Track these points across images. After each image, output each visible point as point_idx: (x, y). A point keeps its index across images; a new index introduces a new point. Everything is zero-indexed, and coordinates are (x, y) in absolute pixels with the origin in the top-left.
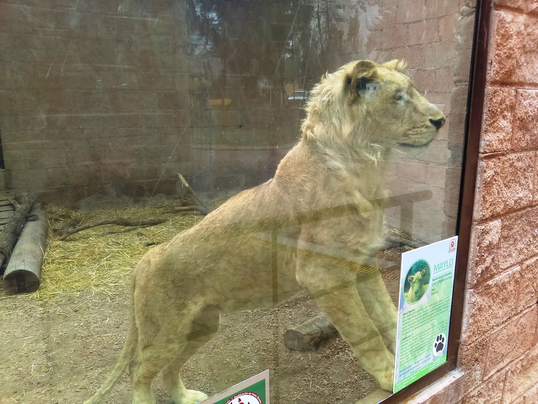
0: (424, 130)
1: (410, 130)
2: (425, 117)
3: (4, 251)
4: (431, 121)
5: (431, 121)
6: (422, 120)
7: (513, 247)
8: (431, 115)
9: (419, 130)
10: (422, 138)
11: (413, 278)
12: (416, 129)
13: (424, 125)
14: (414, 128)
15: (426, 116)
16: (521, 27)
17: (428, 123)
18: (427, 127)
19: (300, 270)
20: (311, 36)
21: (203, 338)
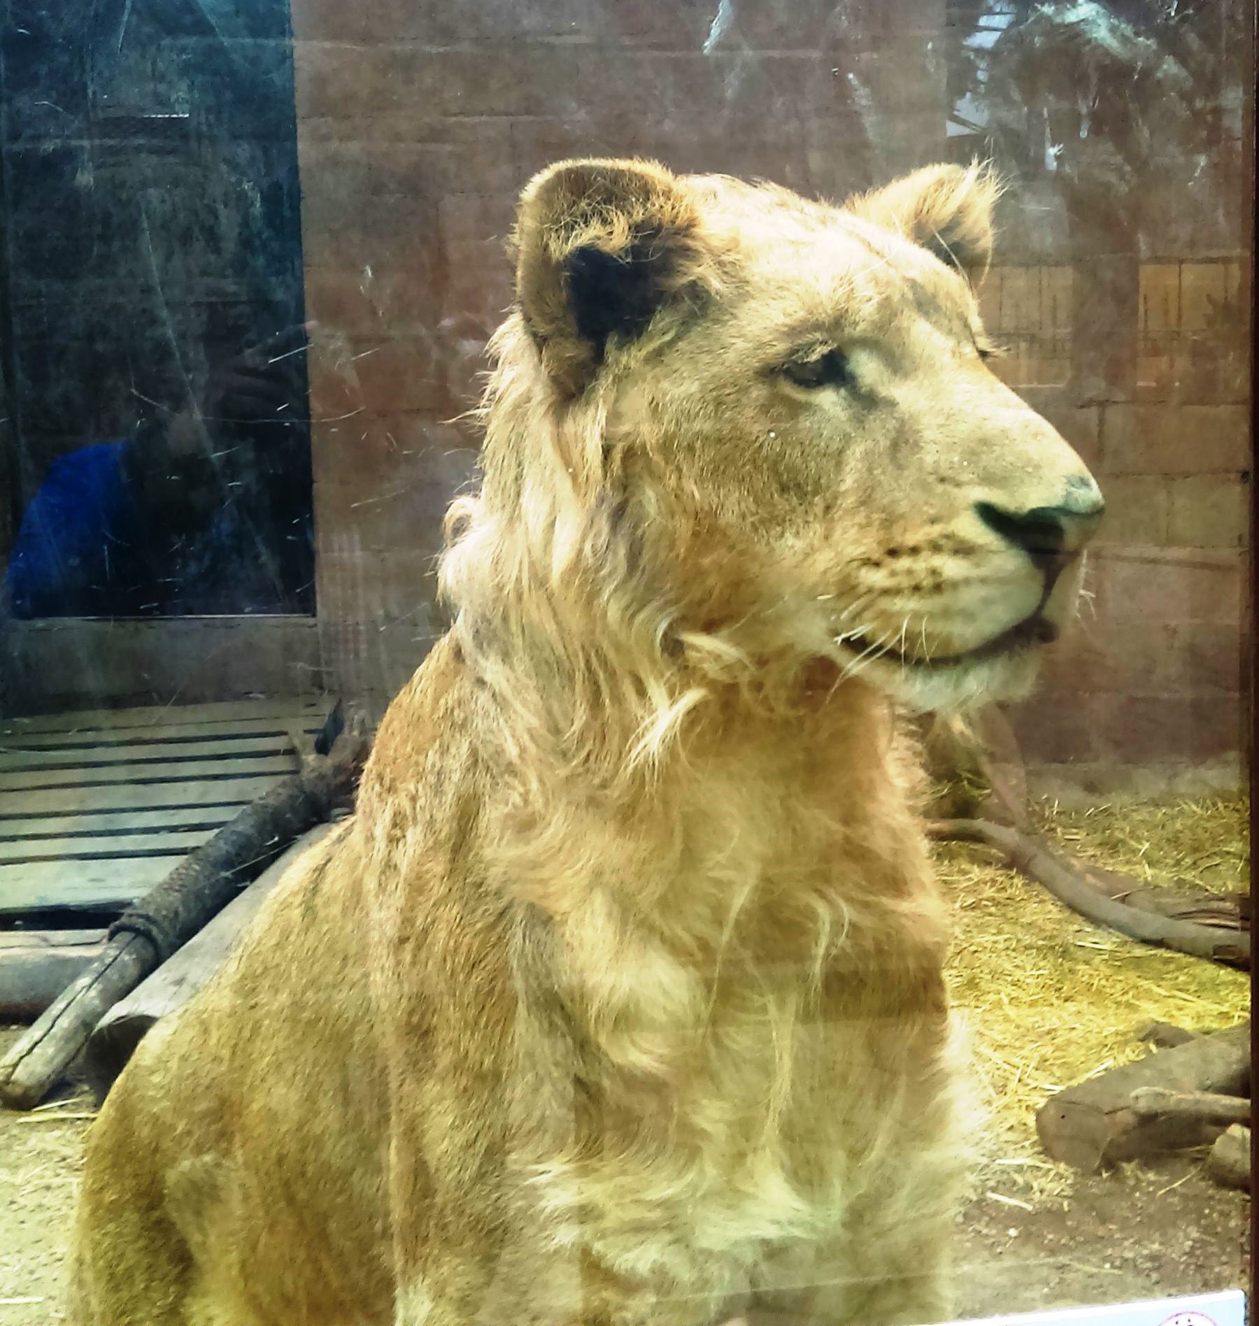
0: (952, 567)
1: (877, 564)
2: (949, 488)
3: (155, 931)
4: (990, 515)
5: (990, 515)
6: (932, 511)
7: (272, 1189)
8: (988, 479)
9: (921, 565)
10: (947, 613)
11: (200, 1128)
12: (904, 563)
13: (947, 537)
14: (893, 553)
15: (958, 485)
16: (436, 1109)
17: (973, 529)
18: (964, 549)
19: (884, 938)
20: (513, 269)
21: (407, 1196)
